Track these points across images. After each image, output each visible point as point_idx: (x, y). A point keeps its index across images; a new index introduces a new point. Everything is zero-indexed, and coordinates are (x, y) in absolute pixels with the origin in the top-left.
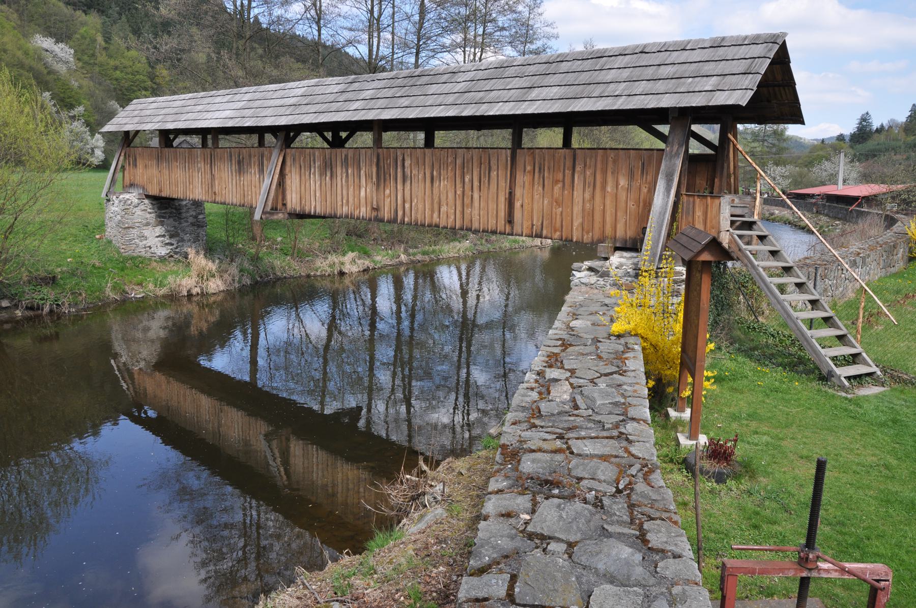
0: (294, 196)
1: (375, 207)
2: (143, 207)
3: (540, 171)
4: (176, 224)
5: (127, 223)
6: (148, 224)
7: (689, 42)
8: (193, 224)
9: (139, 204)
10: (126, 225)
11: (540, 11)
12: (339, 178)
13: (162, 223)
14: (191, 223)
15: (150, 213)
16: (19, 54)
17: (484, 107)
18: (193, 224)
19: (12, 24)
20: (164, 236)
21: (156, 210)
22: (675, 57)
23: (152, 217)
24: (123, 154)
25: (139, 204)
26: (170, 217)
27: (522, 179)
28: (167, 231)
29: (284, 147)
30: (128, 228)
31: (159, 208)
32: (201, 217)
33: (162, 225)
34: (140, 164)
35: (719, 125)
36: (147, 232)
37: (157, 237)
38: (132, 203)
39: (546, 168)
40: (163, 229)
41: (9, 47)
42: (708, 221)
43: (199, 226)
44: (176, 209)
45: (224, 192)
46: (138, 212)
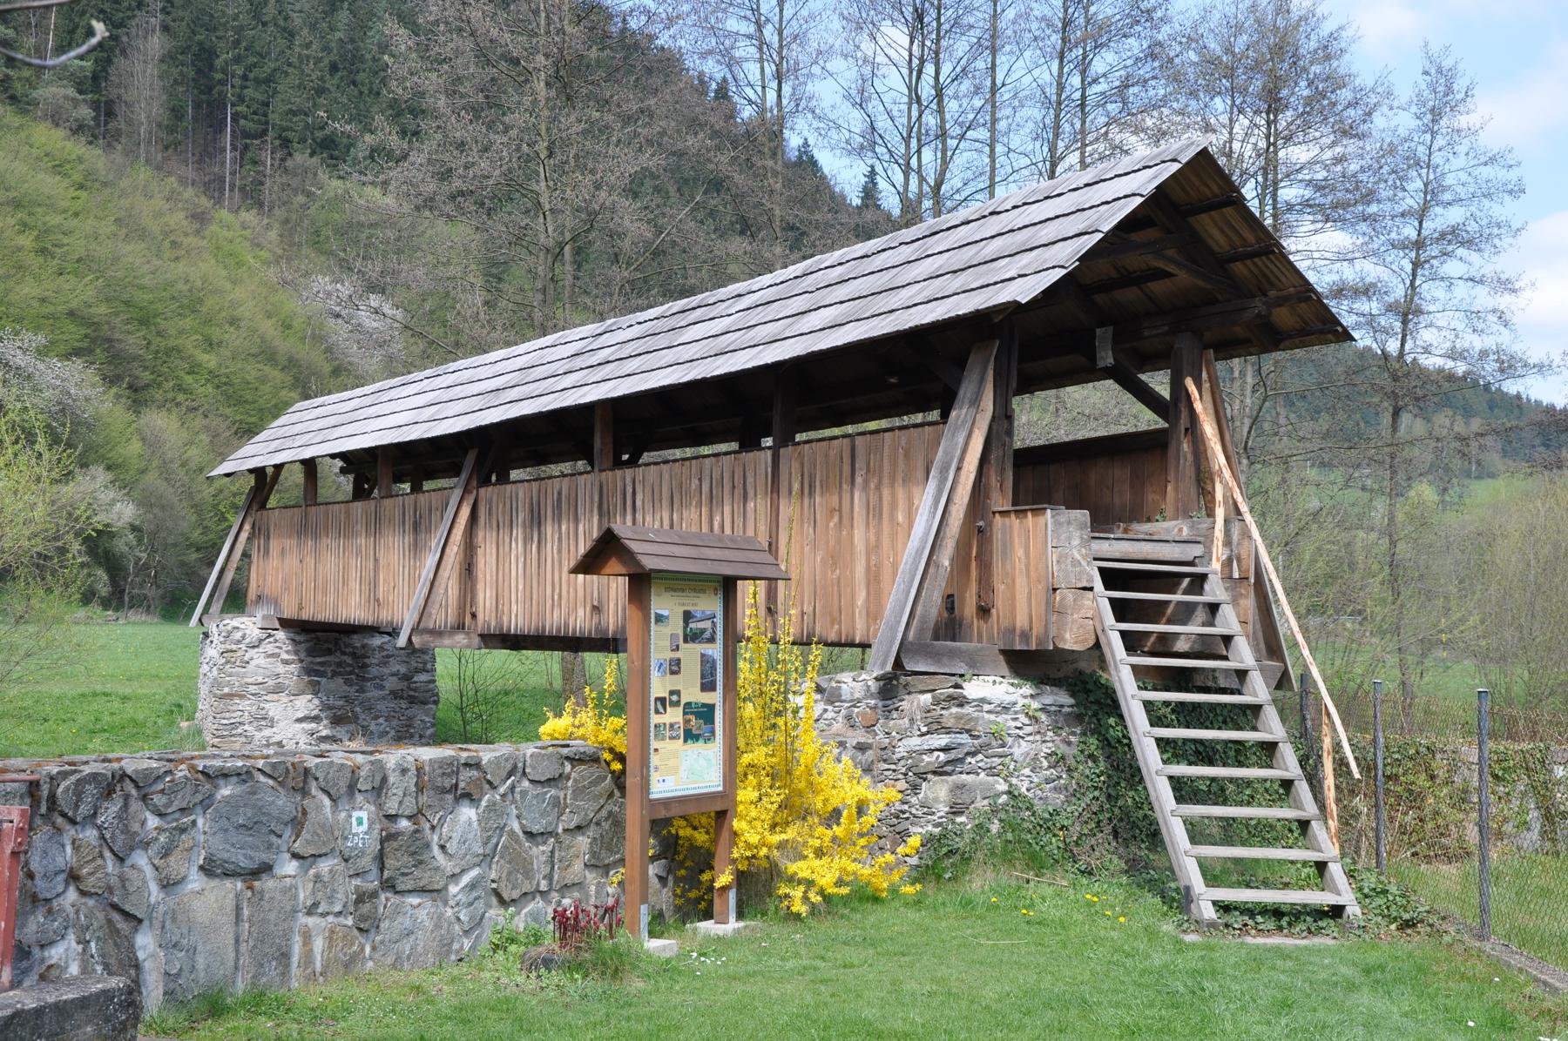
1: (596, 603)
3: (810, 493)
4: (352, 691)
5: (229, 684)
6: (278, 689)
8: (395, 695)
9: (261, 641)
10: (226, 690)
11: (1463, 121)
12: (549, 545)
13: (315, 689)
14: (392, 692)
15: (286, 662)
16: (268, 328)
18: (395, 695)
19: (264, 254)
20: (316, 719)
21: (303, 655)
23: (289, 672)
24: (247, 527)
25: (261, 641)
26: (335, 674)
27: (787, 509)
28: (325, 707)
29: (474, 483)
30: (231, 696)
31: (311, 652)
32: (423, 677)
33: (316, 693)
34: (275, 544)
36: (276, 707)
37: (300, 720)
38: (244, 637)
39: (818, 483)
40: (316, 702)
41: (245, 311)
42: (1032, 568)
43: (413, 701)
44: (354, 655)
45: (391, 599)
46: (258, 658)
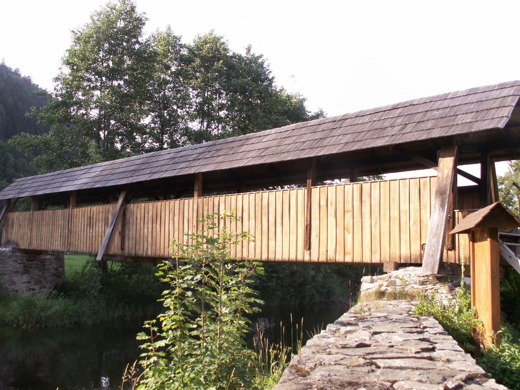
0: (131, 242)
2: (15, 259)
6: (17, 272)
7: (449, 94)
8: (54, 275)
9: (11, 256)
17: (283, 155)
22: (437, 105)
26: (35, 268)
32: (60, 269)
35: (479, 165)
38: (6, 254)
